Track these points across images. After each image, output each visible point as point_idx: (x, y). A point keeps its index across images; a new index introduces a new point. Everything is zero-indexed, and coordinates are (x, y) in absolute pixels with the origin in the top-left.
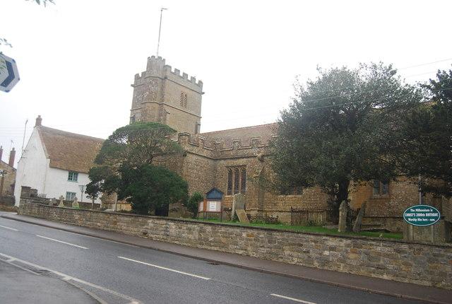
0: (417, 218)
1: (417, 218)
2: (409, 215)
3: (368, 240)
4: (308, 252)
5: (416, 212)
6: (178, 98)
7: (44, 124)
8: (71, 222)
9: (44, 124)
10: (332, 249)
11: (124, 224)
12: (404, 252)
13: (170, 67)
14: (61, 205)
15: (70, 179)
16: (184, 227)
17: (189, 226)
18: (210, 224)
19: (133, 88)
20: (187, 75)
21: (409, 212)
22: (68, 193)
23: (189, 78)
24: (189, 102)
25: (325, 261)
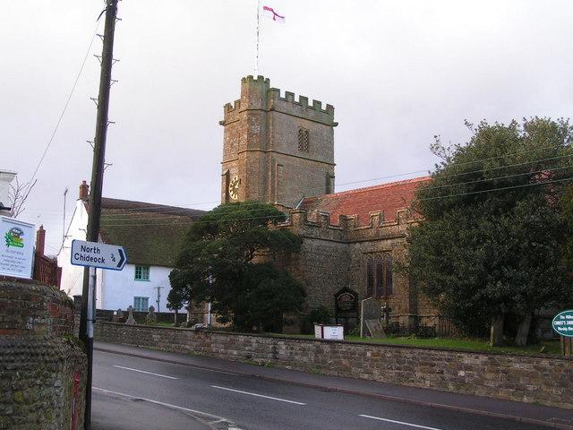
0: (567, 326)
1: (567, 326)
2: (558, 323)
4: (442, 372)
5: (566, 320)
6: (294, 138)
8: (146, 343)
11: (218, 344)
13: (278, 91)
14: (131, 320)
15: (138, 276)
16: (297, 346)
17: (302, 345)
19: (223, 127)
21: (558, 319)
22: (137, 299)
23: (311, 104)
24: (314, 143)
25: (460, 382)
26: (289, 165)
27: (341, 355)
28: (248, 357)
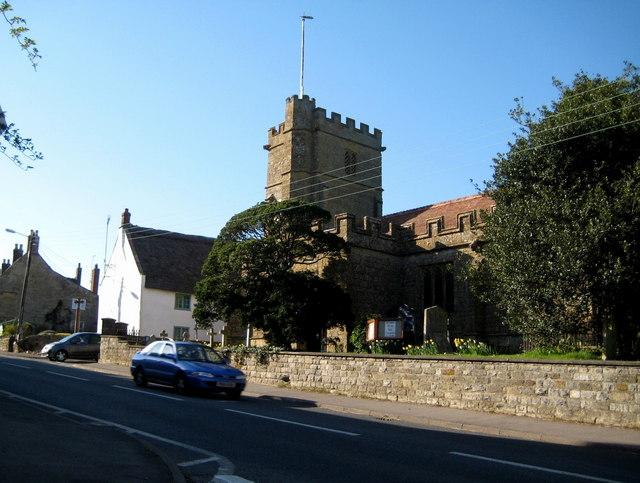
7: (133, 221)
9: (133, 221)
10: (586, 386)
20: (367, 127)
28: (286, 379)
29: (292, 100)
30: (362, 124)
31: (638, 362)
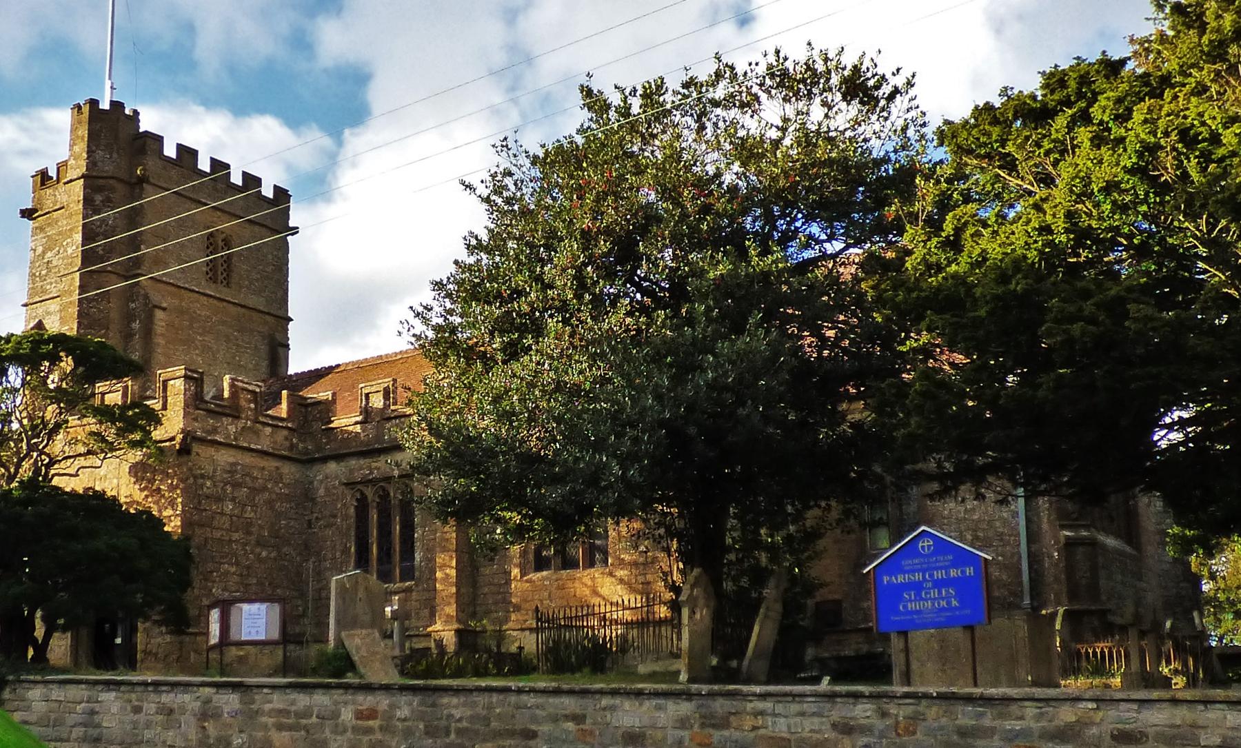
3: (745, 696)
12: (865, 730)
13: (159, 140)
18: (235, 687)
26: (181, 312)
27: (271, 721)
29: (86, 109)
30: (245, 174)
31: (1235, 693)
